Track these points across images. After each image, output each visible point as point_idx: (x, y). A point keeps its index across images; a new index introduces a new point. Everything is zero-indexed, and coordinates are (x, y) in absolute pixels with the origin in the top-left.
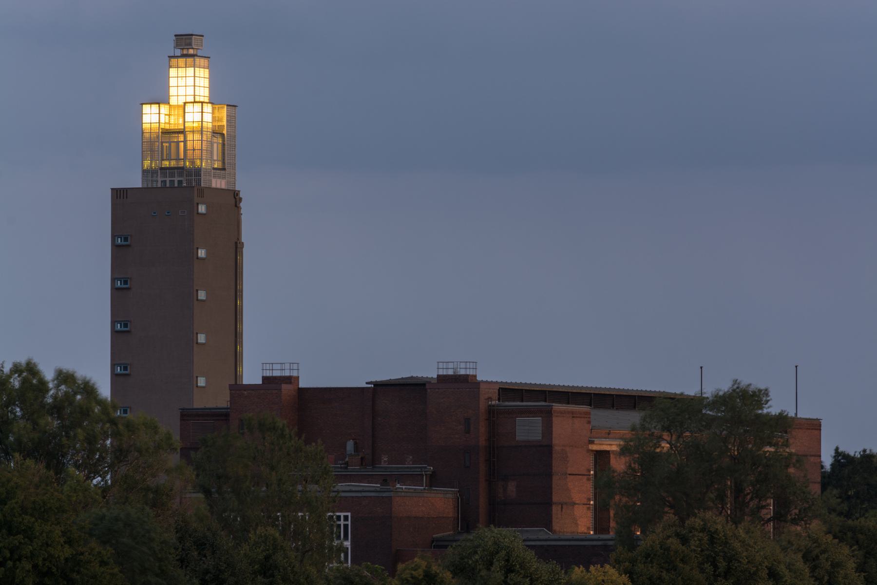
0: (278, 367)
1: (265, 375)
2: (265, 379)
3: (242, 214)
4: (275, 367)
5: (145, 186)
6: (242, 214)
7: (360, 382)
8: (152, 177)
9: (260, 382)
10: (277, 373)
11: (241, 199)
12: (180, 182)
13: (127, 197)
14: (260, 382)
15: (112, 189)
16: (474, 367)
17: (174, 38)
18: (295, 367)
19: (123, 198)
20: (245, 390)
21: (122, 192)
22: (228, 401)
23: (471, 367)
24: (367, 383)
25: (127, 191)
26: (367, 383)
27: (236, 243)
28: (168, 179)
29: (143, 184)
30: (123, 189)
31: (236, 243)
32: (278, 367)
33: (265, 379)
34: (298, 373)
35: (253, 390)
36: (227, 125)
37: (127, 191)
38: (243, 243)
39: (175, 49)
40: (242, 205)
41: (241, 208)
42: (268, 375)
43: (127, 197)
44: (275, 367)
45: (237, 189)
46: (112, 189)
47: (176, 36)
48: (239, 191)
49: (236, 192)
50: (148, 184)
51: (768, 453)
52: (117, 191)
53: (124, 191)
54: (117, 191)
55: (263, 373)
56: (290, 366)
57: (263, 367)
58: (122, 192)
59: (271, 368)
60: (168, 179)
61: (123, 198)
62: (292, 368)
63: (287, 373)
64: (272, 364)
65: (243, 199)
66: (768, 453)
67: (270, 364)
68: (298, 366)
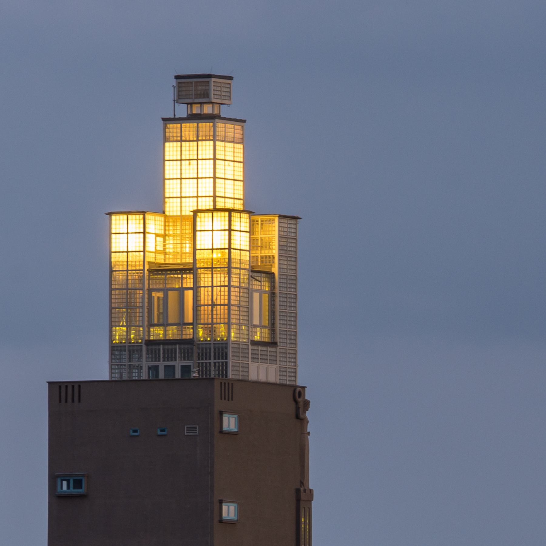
11: (307, 404)
13: (79, 401)
15: (50, 383)
17: (174, 82)
19: (66, 401)
21: (63, 389)
25: (79, 386)
27: (298, 491)
28: (162, 364)
31: (298, 491)
37: (79, 386)
38: (311, 491)
39: (176, 104)
43: (79, 401)
45: (299, 383)
46: (50, 383)
47: (177, 77)
48: (304, 388)
52: (60, 387)
53: (73, 387)
58: (63, 389)
60: (162, 364)
61: (66, 401)
65: (311, 404)
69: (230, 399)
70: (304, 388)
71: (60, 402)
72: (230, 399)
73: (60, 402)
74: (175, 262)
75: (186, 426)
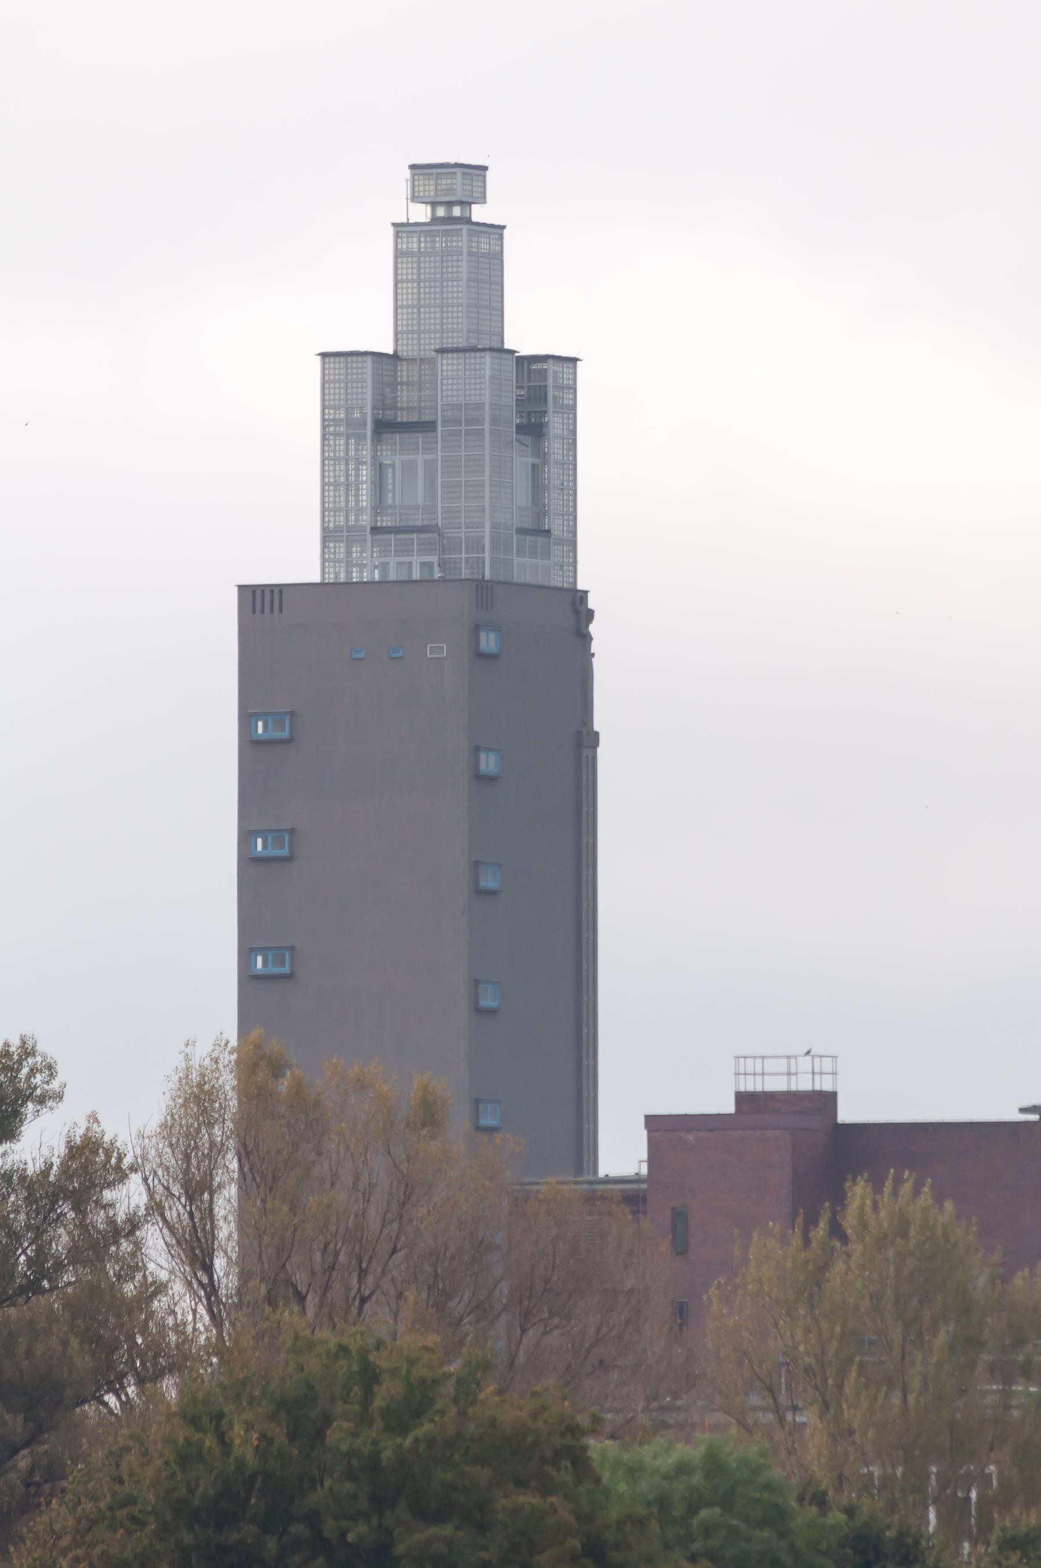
0: (781, 1065)
1: (742, 1089)
2: (742, 1098)
3: (593, 655)
4: (770, 1066)
5: (331, 578)
6: (593, 655)
7: (644, 1133)
8: (349, 553)
9: (728, 1107)
10: (776, 1084)
11: (590, 615)
12: (427, 566)
13: (281, 611)
14: (728, 1107)
16: (742, 1077)
17: (407, 174)
18: (827, 1065)
19: (272, 611)
20: (690, 1131)
22: (640, 1162)
23: (750, 1078)
24: (1023, 1110)
25: (281, 591)
26: (1023, 1110)
27: (579, 734)
28: (393, 560)
29: (323, 573)
30: (272, 587)
31: (579, 734)
32: (805, 1063)
33: (742, 1098)
34: (835, 1082)
35: (712, 1130)
36: (491, 404)
37: (281, 591)
38: (597, 734)
39: (411, 204)
40: (593, 628)
41: (591, 639)
42: (750, 1088)
43: (281, 611)
44: (770, 1066)
48: (586, 592)
49: (579, 594)
50: (336, 574)
51: (260, 1478)
52: (254, 592)
54: (254, 592)
55: (737, 1082)
56: (789, 1065)
57: (737, 1065)
59: (817, 1077)
60: (416, 560)
61: (272, 611)
62: (742, 1070)
63: (804, 1084)
64: (763, 1058)
66: (260, 1478)
67: (754, 1058)
68: (834, 1065)
69: (267, 609)
70: (586, 592)
71: (254, 612)
72: (267, 609)
73: (254, 612)
74: (533, 538)
75: (428, 646)
